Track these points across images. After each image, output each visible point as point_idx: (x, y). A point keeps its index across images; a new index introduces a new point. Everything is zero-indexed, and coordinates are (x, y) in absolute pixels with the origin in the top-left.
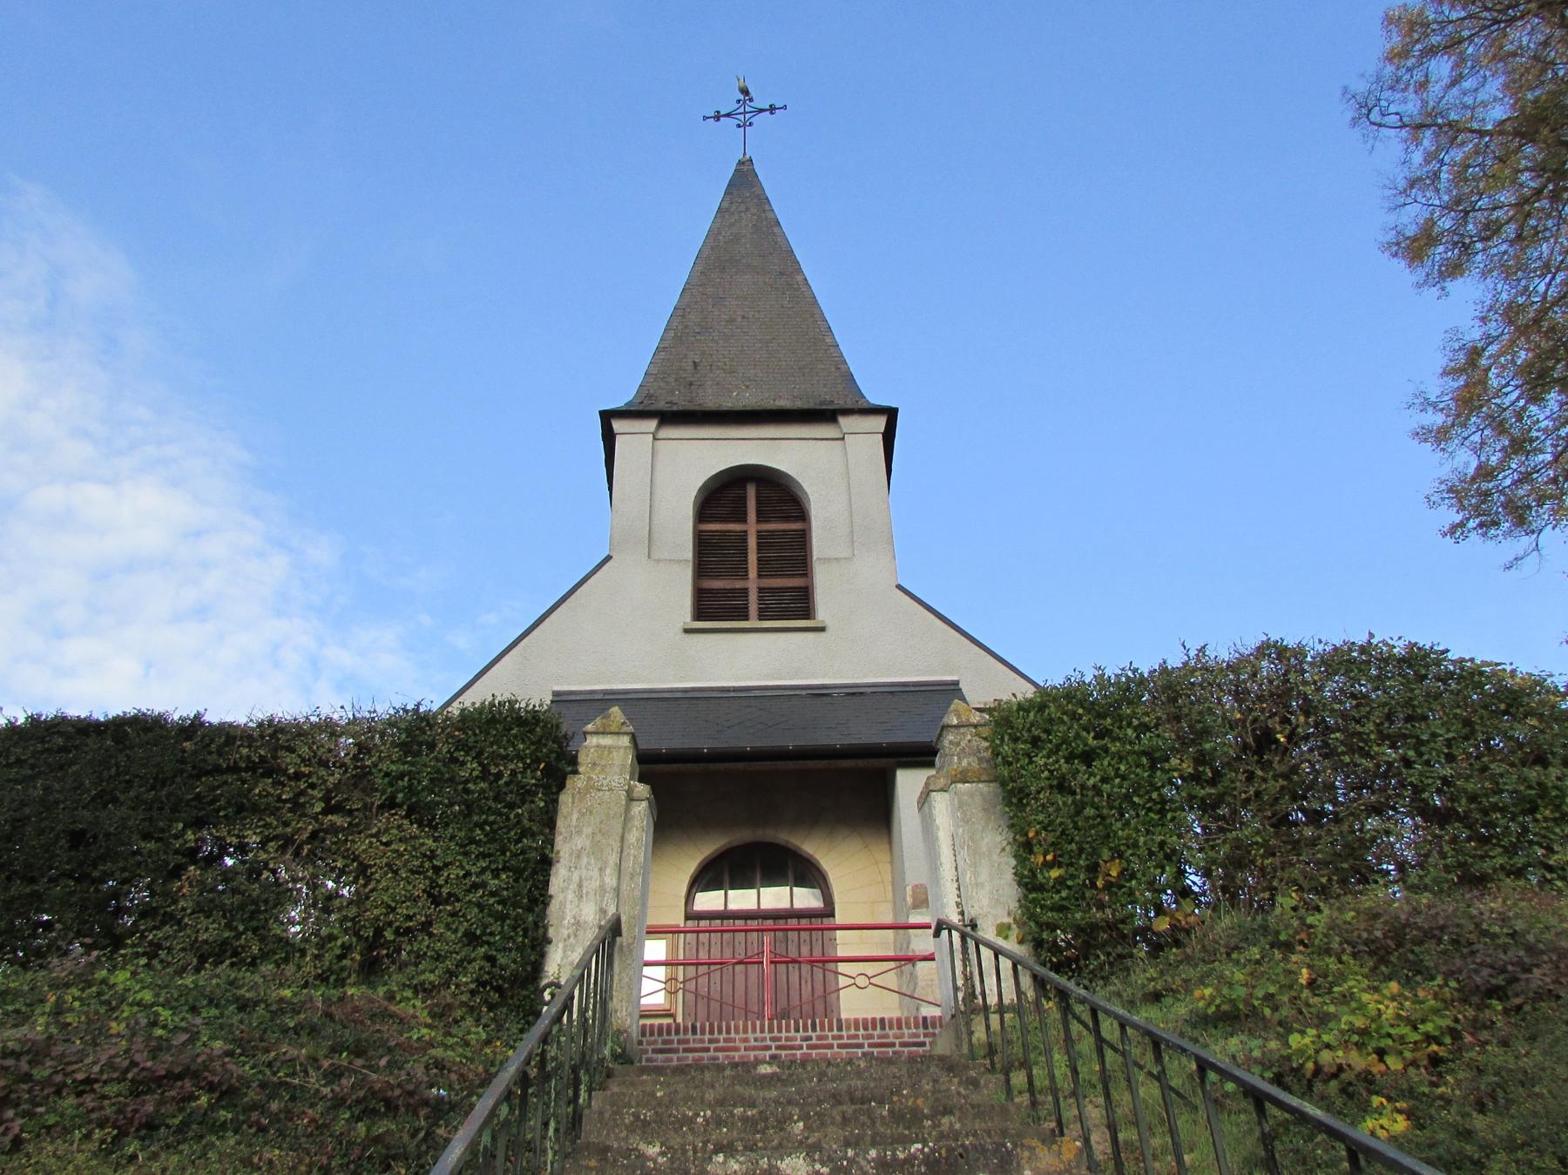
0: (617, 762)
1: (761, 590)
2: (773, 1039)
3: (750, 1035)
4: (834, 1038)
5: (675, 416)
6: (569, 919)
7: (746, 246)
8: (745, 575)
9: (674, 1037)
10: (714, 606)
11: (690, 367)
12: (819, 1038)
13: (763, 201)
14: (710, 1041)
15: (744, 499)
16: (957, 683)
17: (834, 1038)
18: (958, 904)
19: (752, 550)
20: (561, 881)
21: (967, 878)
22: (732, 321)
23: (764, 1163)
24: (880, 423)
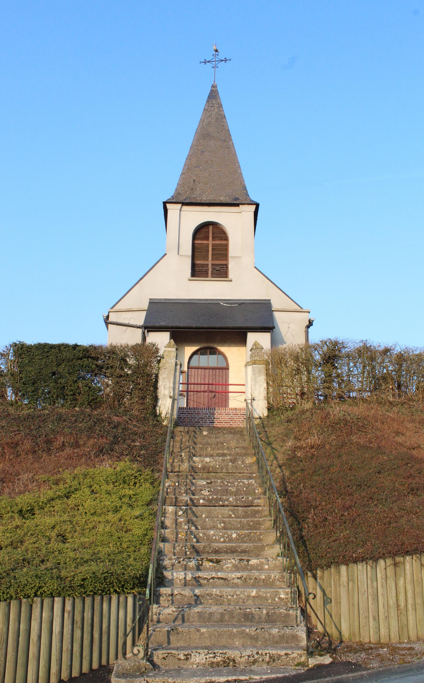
0: (173, 355)
1: (213, 265)
2: (209, 412)
3: (204, 411)
4: (224, 412)
5: (186, 200)
6: (162, 394)
7: (213, 138)
8: (207, 260)
9: (185, 410)
10: (197, 271)
11: (192, 182)
12: (220, 412)
13: (220, 106)
14: (194, 412)
15: (208, 232)
16: (270, 300)
17: (224, 412)
18: (251, 393)
19: (209, 252)
20: (160, 384)
21: (253, 388)
22: (207, 162)
23: (202, 459)
24: (254, 207)
